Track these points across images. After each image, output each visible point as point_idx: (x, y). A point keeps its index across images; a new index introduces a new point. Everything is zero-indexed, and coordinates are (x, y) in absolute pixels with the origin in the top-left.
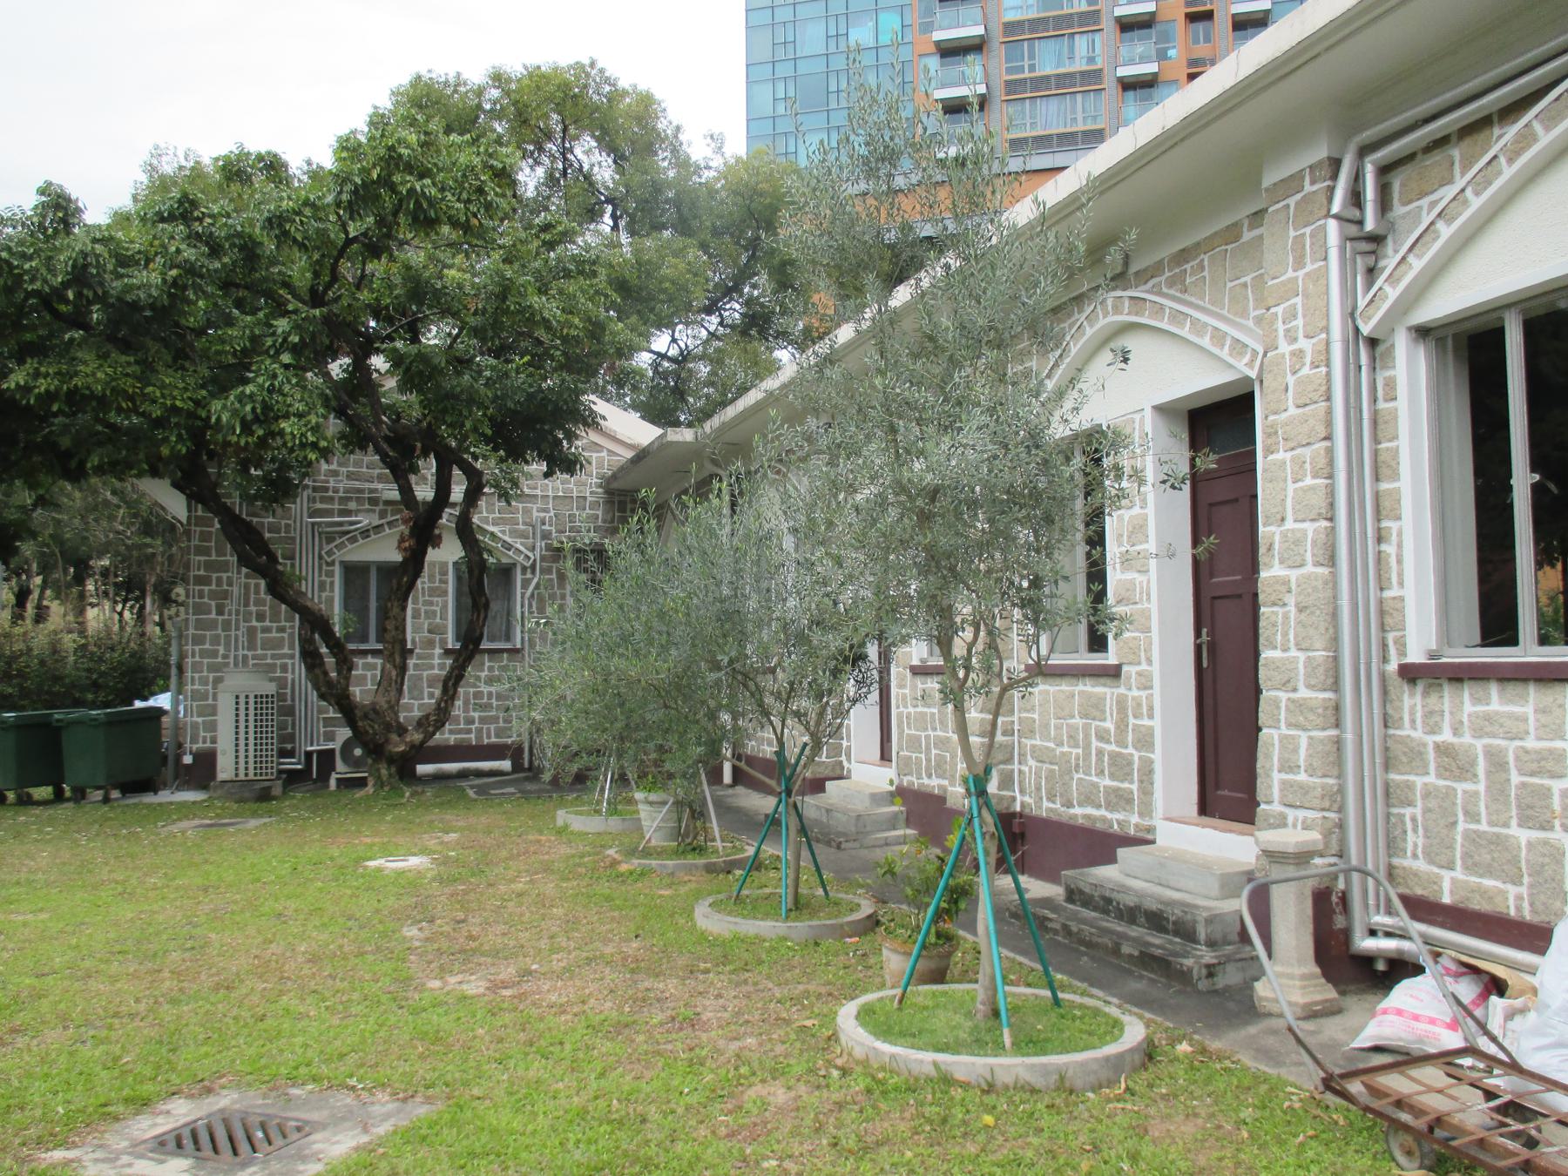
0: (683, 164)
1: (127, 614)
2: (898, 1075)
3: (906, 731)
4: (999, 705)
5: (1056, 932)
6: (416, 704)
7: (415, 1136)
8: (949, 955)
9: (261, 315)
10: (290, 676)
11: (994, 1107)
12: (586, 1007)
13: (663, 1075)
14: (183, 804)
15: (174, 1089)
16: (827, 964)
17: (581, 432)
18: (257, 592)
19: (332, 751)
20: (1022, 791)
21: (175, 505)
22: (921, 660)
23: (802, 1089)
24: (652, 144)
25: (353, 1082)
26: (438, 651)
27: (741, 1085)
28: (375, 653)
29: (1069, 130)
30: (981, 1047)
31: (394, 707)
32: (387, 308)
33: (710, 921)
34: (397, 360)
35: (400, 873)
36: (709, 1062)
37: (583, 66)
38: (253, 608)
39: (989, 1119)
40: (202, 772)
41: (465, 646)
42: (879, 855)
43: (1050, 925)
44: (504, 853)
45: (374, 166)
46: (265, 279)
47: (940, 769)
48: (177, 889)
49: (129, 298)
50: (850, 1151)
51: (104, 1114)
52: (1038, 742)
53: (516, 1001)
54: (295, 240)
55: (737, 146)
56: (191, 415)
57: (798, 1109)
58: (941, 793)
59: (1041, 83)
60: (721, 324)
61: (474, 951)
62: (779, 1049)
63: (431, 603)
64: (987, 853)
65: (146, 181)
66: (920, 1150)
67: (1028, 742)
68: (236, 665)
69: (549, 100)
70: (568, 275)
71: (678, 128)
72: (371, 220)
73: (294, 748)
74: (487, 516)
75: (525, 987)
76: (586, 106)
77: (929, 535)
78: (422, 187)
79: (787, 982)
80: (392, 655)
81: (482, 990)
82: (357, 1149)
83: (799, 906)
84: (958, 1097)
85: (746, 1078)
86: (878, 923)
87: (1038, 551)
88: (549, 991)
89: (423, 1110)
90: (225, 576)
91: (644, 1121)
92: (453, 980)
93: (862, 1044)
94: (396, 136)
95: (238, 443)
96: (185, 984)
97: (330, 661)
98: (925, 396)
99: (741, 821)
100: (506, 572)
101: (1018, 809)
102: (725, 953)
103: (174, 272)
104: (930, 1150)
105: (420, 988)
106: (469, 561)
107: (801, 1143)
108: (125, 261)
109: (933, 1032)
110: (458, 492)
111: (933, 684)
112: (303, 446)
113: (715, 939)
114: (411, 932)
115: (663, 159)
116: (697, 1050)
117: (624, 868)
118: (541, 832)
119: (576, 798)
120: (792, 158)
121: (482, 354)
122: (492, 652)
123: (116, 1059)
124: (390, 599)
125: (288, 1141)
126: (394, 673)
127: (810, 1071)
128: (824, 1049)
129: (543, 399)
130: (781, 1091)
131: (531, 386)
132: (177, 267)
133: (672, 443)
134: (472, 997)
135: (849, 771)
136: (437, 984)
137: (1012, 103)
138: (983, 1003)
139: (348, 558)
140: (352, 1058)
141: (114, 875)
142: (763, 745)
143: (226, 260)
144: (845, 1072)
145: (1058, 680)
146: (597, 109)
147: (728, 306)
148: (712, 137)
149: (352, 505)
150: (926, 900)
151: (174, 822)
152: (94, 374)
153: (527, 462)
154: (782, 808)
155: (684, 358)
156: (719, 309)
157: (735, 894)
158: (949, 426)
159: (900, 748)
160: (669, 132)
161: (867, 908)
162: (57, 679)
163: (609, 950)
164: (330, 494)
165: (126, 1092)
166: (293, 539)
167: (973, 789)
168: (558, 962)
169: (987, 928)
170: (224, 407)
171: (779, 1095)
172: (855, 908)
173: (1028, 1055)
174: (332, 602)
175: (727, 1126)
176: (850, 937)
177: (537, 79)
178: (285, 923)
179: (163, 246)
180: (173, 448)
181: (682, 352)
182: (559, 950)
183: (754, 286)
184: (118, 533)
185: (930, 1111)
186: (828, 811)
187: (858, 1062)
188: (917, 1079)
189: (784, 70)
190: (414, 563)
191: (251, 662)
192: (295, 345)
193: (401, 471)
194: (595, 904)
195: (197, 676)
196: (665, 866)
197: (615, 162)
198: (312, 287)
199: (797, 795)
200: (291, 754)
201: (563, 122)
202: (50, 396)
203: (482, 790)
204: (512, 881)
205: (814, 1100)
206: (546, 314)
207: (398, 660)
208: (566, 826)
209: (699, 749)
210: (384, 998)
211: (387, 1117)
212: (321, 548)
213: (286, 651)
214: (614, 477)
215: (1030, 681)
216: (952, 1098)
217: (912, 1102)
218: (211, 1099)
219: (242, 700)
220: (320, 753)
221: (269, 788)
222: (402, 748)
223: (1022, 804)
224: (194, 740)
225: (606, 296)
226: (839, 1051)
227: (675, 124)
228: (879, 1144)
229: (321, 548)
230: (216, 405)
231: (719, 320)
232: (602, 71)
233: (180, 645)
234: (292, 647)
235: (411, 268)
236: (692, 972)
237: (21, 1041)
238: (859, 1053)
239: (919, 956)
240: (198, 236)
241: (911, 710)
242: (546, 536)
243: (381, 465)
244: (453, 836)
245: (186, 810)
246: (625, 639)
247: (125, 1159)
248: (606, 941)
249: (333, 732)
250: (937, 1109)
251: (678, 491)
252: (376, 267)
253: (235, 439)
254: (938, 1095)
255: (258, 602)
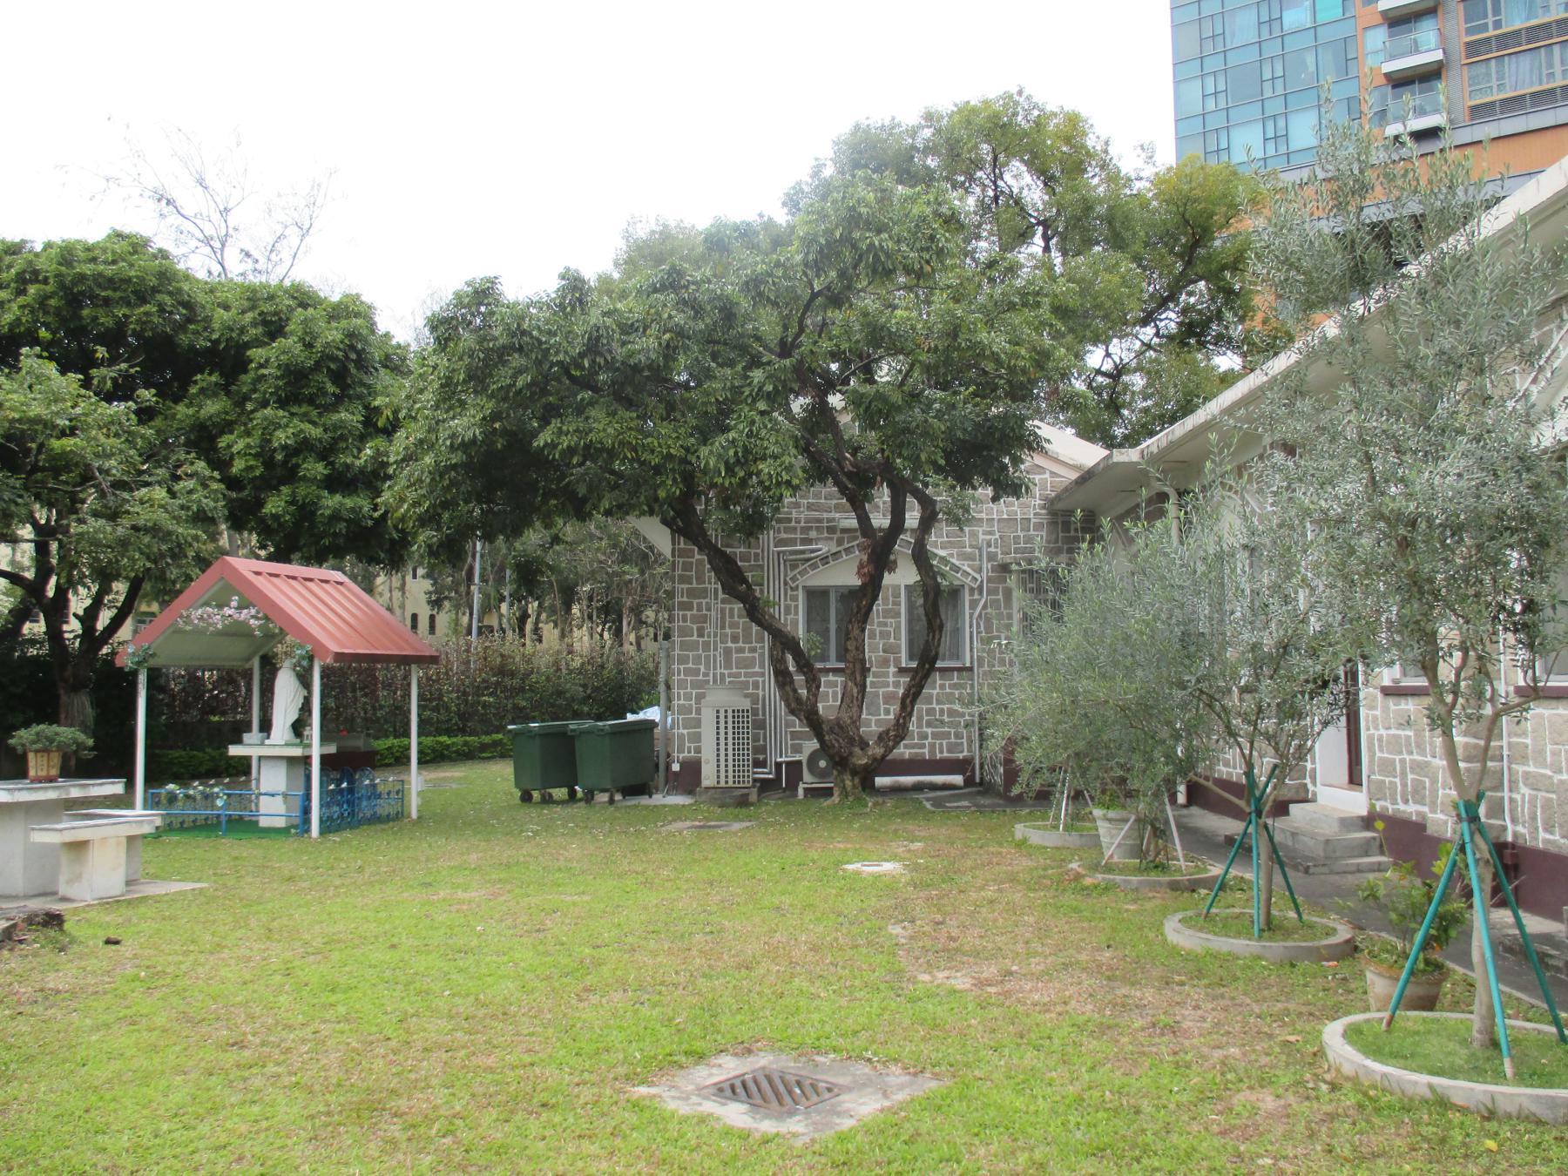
0: (1114, 178)
1: (606, 635)
2: (1391, 1094)
3: (1378, 754)
4: (1490, 731)
5: (1558, 970)
6: (876, 719)
7: (934, 1105)
8: (1438, 983)
9: (739, 368)
10: (761, 693)
11: (1496, 1134)
12: (1068, 1008)
13: (1151, 1073)
14: (675, 807)
15: (722, 1047)
16: (1306, 985)
17: (1025, 455)
18: (732, 616)
19: (799, 763)
20: (1514, 821)
21: (658, 536)
22: (1394, 681)
23: (1291, 1098)
24: (1082, 162)
25: (869, 1055)
26: (892, 669)
27: (1229, 1089)
28: (835, 671)
29: (1545, 87)
30: (1479, 1074)
31: (856, 722)
32: (844, 352)
33: (1178, 934)
34: (855, 401)
35: (878, 877)
36: (1194, 1067)
37: (1011, 97)
38: (728, 630)
39: (1491, 1144)
40: (689, 779)
41: (921, 665)
42: (1351, 880)
43: (1552, 962)
44: (969, 863)
45: (837, 227)
46: (742, 336)
47: (1418, 794)
48: (687, 881)
49: (632, 362)
50: (1345, 1159)
51: (670, 1062)
52: (1531, 769)
53: (1002, 998)
54: (768, 299)
55: (1167, 157)
56: (684, 461)
57: (1288, 1116)
58: (1420, 820)
59: (1511, 39)
60: (1157, 335)
61: (957, 950)
62: (1264, 1060)
63: (885, 625)
64: (1481, 879)
65: (624, 248)
66: (1418, 1165)
67: (1520, 769)
68: (715, 681)
69: (980, 130)
70: (1012, 307)
71: (1107, 143)
72: (833, 274)
73: (765, 759)
74: (940, 544)
75: (1008, 986)
76: (1015, 134)
77: (1412, 562)
78: (881, 241)
79: (1264, 999)
80: (853, 673)
81: (968, 986)
82: (882, 1110)
83: (1271, 926)
84: (1456, 1121)
85: (1233, 1084)
86: (1356, 949)
87: (1532, 575)
88: (1031, 991)
89: (933, 1084)
90: (704, 601)
91: (1138, 1112)
92: (941, 975)
93: (1352, 1062)
94: (856, 196)
95: (722, 484)
96: (712, 962)
97: (799, 679)
98: (1403, 428)
99: (1200, 842)
100: (955, 593)
101: (1510, 839)
102: (1197, 968)
103: (667, 336)
104: (1429, 1166)
105: (913, 980)
106: (924, 585)
107: (1295, 1147)
108: (627, 329)
109: (1426, 1056)
110: (912, 518)
111: (1410, 706)
112: (779, 484)
113: (1188, 954)
114: (896, 930)
115: (1094, 180)
116: (1182, 1054)
117: (1088, 881)
118: (1001, 845)
119: (1030, 813)
120: (1224, 157)
121: (930, 387)
122: (943, 670)
123: (670, 1020)
124: (850, 622)
125: (821, 1098)
126: (855, 690)
127: (1297, 1083)
128: (1310, 1064)
129: (990, 428)
130: (1269, 1098)
131: (978, 415)
132: (670, 331)
133: (1117, 464)
134: (961, 991)
135: (1315, 794)
136: (926, 977)
137: (1474, 66)
138: (1480, 1032)
139: (810, 583)
140: (864, 1035)
141: (632, 867)
142: (1229, 766)
143: (708, 321)
144: (1334, 1087)
145: (1554, 703)
146: (1026, 134)
147: (1163, 316)
148: (1142, 147)
149: (813, 534)
150: (1413, 925)
151: (670, 822)
152: (604, 430)
153: (974, 488)
154: (1251, 829)
155: (1119, 371)
156: (1154, 320)
157: (1205, 911)
158: (1433, 454)
159: (1372, 772)
160: (1098, 148)
161: (1343, 933)
162: (560, 693)
163: (1083, 957)
164: (793, 524)
165: (685, 1047)
166: (761, 567)
167: (1464, 815)
168: (1036, 965)
169: (1483, 956)
170: (711, 452)
171: (1268, 1102)
172: (1331, 932)
173: (1532, 1086)
174: (797, 623)
175: (1218, 1125)
176: (1328, 960)
177: (967, 114)
178: (784, 915)
179: (657, 313)
180: (668, 491)
181: (1116, 367)
182: (1036, 954)
183: (1190, 294)
184: (601, 562)
185: (1428, 1131)
186: (1294, 834)
187: (1347, 1079)
188: (1411, 1100)
189: (1214, 64)
190: (871, 588)
191: (728, 680)
192: (769, 393)
193: (858, 501)
194: (1065, 915)
195: (682, 692)
196: (1128, 882)
197: (1046, 184)
198: (782, 339)
199: (1267, 817)
200: (762, 764)
201: (994, 150)
202: (571, 451)
203: (938, 803)
204: (982, 888)
205: (1304, 1109)
206: (995, 349)
207: (858, 678)
208: (1025, 840)
209: (1166, 769)
210: (882, 987)
211: (902, 1089)
212: (786, 575)
213: (757, 669)
214: (1058, 498)
215: (1525, 706)
216: (1450, 1121)
217: (1407, 1120)
218: (751, 1059)
219: (722, 715)
220: (788, 764)
221: (747, 795)
222: (864, 761)
223: (1515, 834)
224: (681, 750)
225: (1051, 325)
226: (1326, 1067)
227: (1103, 138)
228: (1375, 1156)
229: (786, 575)
230: (704, 451)
231: (1154, 331)
232: (1028, 98)
233: (668, 662)
234: (762, 666)
235: (868, 314)
236: (1167, 983)
237: (594, 999)
238: (1347, 1069)
239: (1407, 982)
240: (685, 302)
241: (1383, 732)
242: (991, 557)
243: (839, 495)
244: (918, 845)
245: (678, 813)
246: (1091, 661)
247: (694, 1099)
248: (1079, 950)
249: (800, 745)
250: (1435, 1130)
251: (1120, 510)
252: (836, 315)
253: (721, 480)
254: (1435, 1116)
255: (734, 625)
